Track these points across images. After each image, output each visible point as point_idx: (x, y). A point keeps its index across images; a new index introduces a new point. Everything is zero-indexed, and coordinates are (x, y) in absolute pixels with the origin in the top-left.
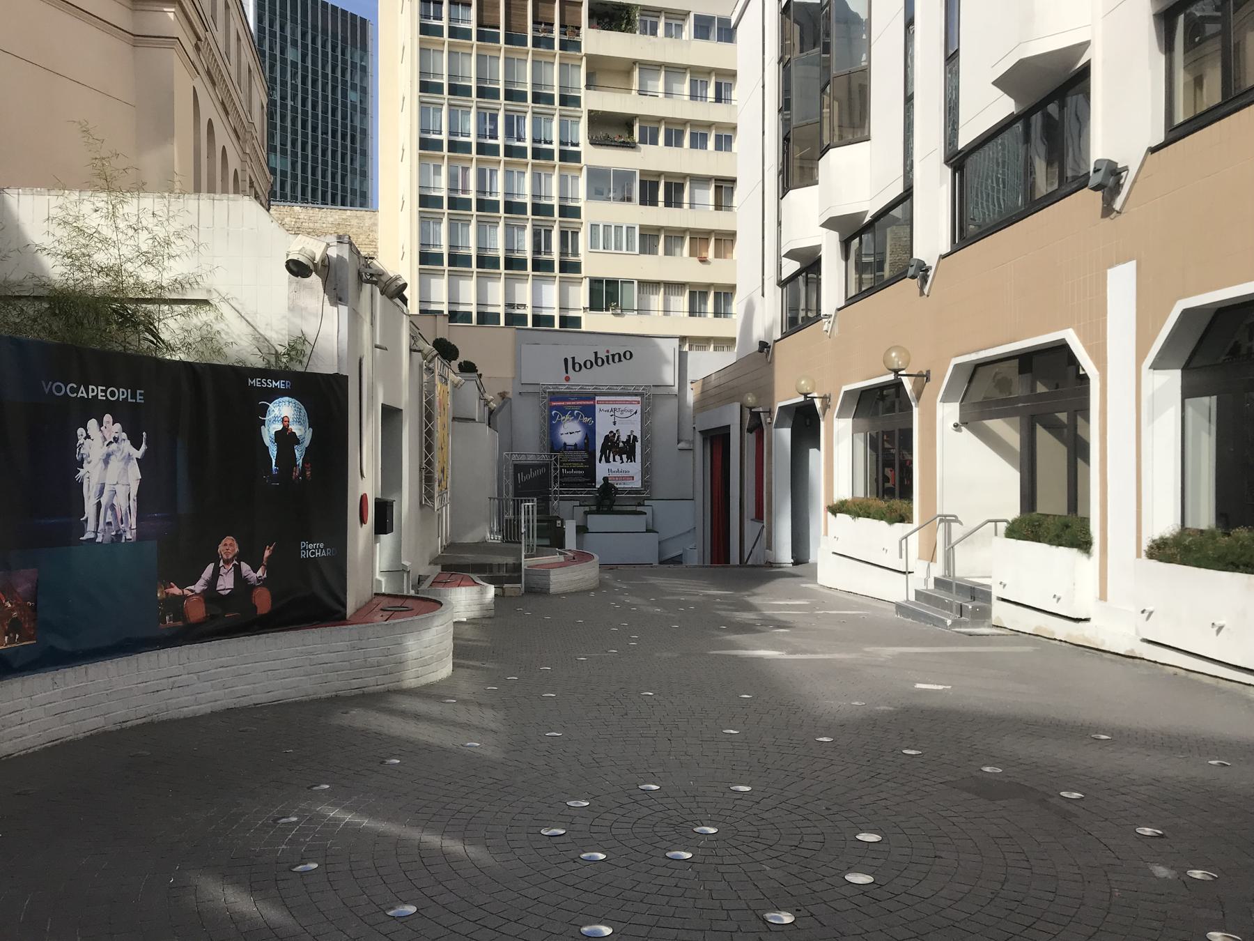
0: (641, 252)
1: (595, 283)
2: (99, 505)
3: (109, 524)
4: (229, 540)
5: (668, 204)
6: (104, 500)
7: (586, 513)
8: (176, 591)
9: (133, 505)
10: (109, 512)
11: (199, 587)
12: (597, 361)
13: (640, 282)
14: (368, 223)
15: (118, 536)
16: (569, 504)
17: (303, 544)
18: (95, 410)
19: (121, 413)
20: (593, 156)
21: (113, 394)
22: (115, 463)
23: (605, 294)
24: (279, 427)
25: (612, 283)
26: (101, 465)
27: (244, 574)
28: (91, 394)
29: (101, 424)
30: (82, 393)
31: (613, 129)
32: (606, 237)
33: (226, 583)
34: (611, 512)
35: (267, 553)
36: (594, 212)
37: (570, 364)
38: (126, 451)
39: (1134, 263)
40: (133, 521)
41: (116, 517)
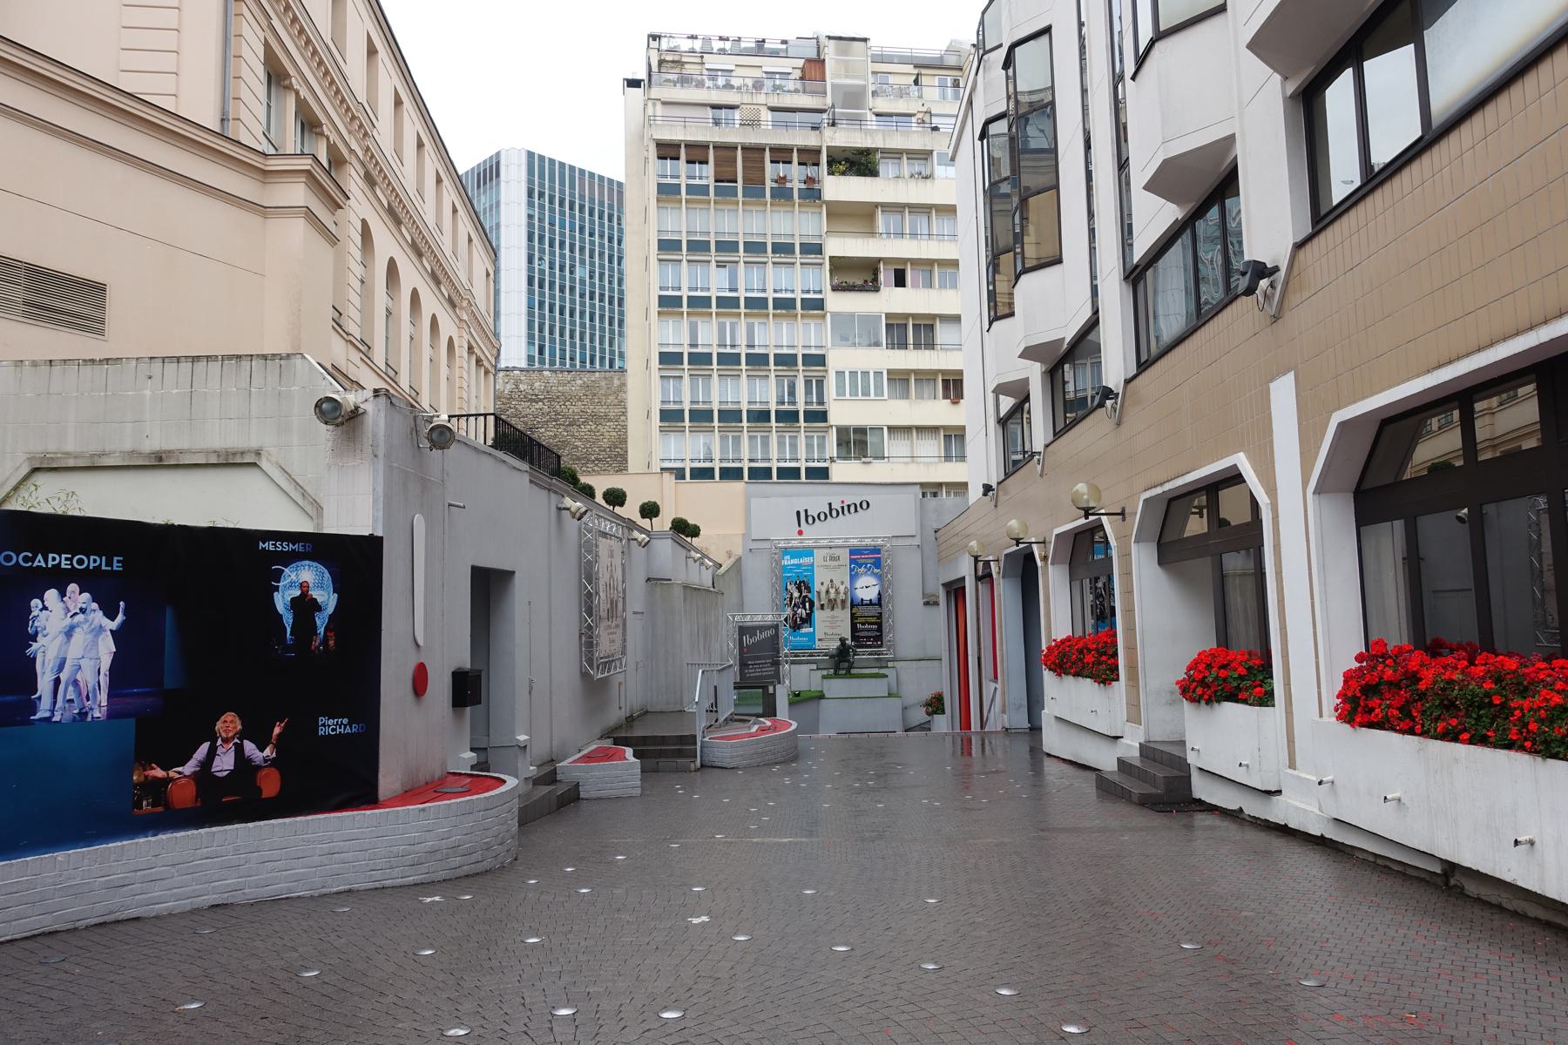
0: (890, 397)
1: (842, 431)
2: (57, 682)
3: (71, 701)
4: (229, 716)
5: (917, 346)
6: (64, 676)
7: (824, 677)
8: (159, 773)
9: (104, 681)
10: (71, 688)
11: (189, 768)
12: (831, 512)
13: (890, 428)
14: (616, 382)
15: (83, 714)
16: (805, 668)
17: (322, 720)
18: (59, 580)
19: (88, 580)
20: (838, 303)
21: (80, 562)
22: (79, 637)
23: (856, 442)
24: (298, 593)
25: (861, 431)
26: (62, 638)
27: (247, 753)
28: (50, 563)
29: (63, 594)
30: (39, 561)
31: (860, 275)
32: (858, 383)
33: (224, 763)
34: (849, 675)
35: (277, 730)
36: (841, 359)
37: (803, 517)
38: (96, 622)
39: (1291, 375)
40: (103, 698)
41: (80, 694)
